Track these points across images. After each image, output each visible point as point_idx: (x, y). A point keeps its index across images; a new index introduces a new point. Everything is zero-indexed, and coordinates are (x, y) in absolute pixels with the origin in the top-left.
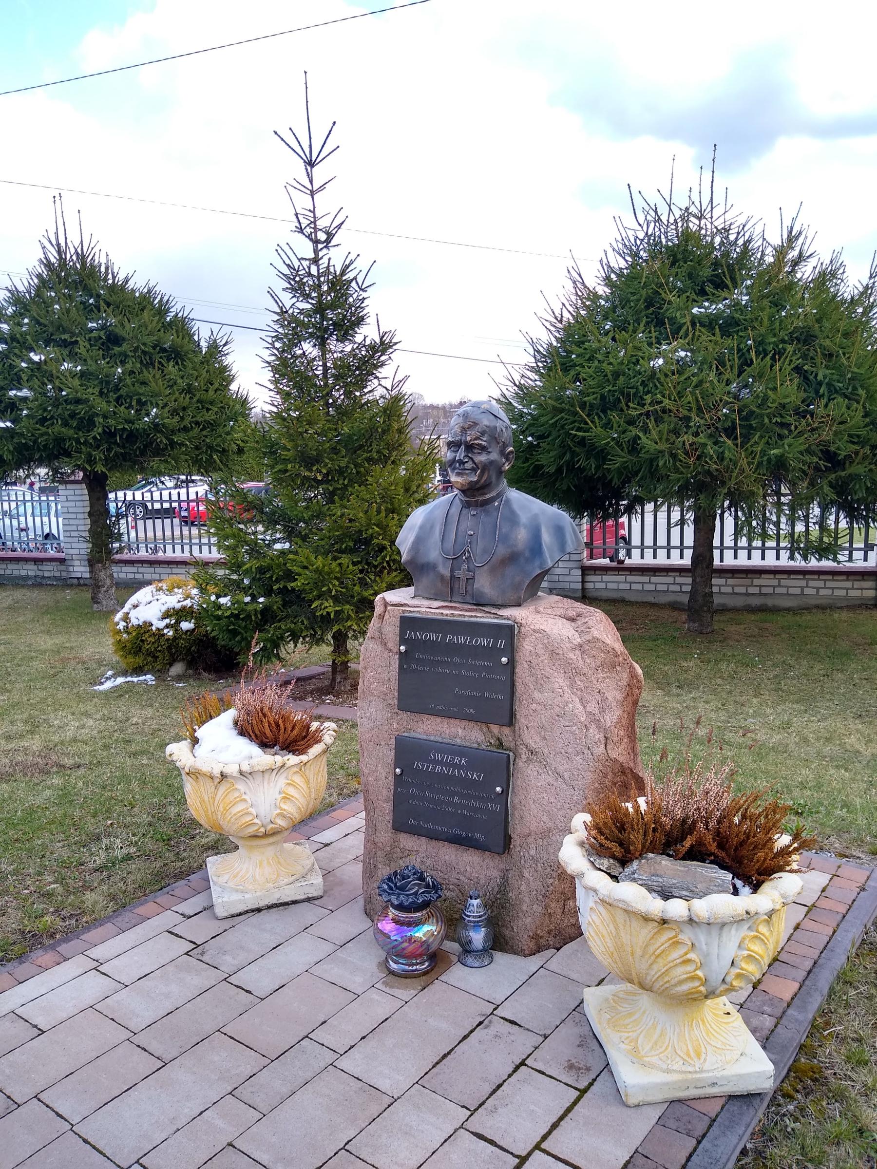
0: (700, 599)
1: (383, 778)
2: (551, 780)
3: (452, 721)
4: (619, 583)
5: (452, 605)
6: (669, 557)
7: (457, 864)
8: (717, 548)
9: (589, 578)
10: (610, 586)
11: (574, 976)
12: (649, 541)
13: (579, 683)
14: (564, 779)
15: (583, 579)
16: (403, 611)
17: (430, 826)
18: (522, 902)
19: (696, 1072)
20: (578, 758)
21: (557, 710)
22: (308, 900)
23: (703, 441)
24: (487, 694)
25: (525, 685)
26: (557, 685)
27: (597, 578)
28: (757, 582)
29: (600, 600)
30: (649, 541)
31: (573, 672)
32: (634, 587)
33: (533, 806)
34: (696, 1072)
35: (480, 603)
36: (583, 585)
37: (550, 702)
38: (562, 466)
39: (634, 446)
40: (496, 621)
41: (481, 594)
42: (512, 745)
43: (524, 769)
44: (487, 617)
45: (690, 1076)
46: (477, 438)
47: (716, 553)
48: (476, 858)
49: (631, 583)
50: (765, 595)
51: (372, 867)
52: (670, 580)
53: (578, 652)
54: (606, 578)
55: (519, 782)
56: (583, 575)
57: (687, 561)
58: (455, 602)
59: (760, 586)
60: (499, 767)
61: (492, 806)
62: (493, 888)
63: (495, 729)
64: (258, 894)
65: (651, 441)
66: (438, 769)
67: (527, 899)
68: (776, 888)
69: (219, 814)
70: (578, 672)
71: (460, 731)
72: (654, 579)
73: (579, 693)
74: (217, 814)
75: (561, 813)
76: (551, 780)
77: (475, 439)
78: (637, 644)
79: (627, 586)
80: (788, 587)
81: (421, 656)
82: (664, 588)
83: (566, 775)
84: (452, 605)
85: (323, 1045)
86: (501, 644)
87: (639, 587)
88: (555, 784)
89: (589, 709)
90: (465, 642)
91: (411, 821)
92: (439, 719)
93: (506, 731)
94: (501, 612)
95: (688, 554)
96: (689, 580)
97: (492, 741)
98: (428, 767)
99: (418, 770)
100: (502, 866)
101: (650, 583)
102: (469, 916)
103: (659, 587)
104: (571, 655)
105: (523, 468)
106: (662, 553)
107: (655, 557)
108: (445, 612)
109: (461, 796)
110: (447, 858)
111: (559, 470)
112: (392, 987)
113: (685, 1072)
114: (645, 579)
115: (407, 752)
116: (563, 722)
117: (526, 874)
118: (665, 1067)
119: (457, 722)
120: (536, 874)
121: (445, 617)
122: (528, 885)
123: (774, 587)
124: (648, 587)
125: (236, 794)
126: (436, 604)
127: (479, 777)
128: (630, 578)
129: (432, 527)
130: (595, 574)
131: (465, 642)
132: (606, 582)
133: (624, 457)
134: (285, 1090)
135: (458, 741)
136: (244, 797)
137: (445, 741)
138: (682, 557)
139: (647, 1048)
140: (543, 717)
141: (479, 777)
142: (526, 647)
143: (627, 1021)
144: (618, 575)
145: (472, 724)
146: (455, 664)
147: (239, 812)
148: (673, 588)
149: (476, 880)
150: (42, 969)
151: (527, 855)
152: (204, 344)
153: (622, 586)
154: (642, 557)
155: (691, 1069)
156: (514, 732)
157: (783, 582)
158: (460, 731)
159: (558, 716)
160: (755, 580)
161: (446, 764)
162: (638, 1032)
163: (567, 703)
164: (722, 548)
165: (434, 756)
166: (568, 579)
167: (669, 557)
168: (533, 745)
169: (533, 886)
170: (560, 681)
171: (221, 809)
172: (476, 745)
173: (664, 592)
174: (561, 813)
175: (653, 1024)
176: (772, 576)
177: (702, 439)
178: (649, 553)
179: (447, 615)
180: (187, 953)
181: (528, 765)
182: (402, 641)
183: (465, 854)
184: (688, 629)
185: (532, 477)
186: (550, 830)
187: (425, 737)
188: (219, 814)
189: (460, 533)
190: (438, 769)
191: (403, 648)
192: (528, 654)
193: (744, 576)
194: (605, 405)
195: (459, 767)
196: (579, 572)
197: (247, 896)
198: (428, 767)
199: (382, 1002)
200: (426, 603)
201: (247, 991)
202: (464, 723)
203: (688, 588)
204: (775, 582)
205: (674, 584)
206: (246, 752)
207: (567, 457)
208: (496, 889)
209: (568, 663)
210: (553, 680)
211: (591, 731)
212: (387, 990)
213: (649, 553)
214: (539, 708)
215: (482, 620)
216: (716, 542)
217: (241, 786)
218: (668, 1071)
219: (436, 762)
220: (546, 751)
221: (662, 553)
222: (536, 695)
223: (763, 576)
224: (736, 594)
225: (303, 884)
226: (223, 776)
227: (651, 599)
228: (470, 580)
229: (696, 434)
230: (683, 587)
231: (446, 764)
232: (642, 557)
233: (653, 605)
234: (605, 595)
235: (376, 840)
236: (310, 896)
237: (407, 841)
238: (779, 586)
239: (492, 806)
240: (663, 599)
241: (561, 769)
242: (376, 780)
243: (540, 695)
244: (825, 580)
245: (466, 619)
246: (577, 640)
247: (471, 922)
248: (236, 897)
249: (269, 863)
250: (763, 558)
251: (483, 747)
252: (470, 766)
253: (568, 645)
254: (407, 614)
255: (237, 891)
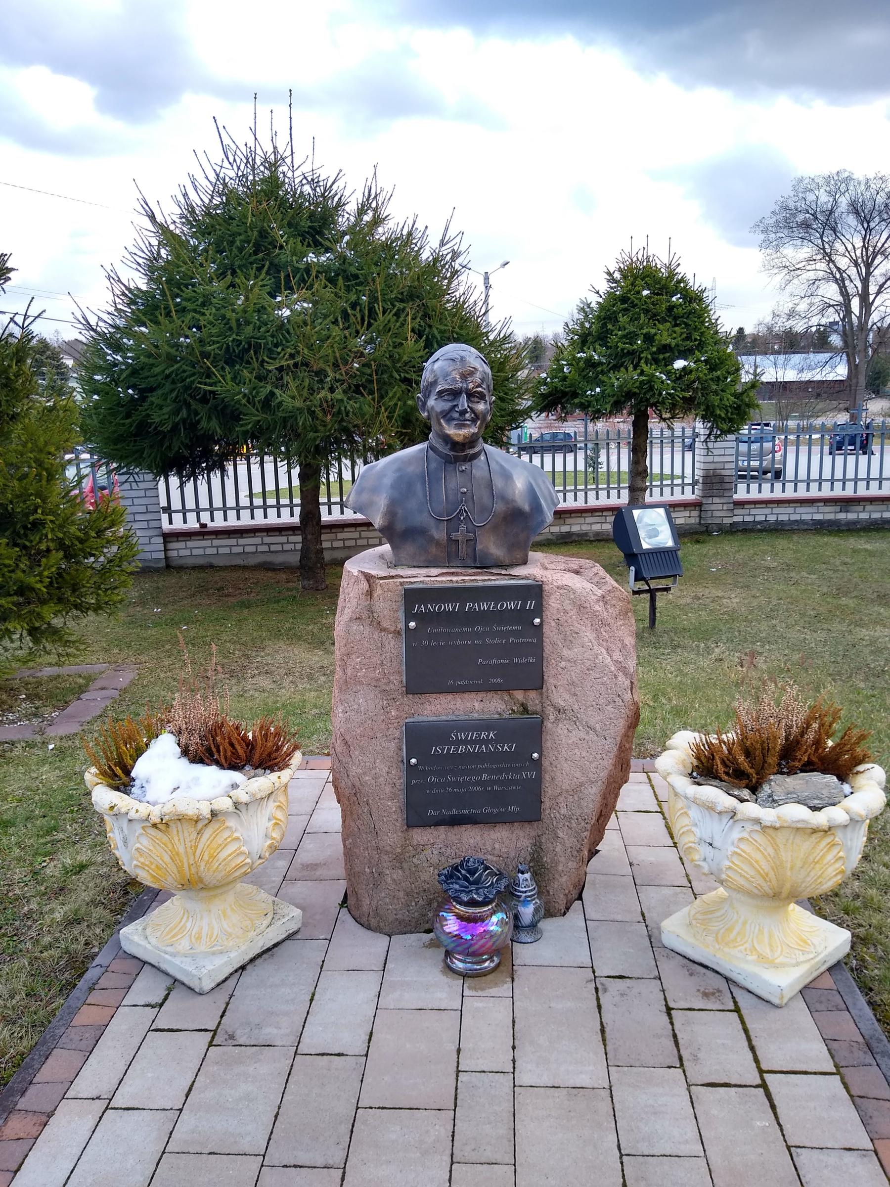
0: (313, 556)
1: (385, 774)
2: (582, 734)
3: (466, 695)
4: (204, 548)
5: (453, 570)
6: (253, 517)
7: (484, 845)
8: (297, 505)
9: (172, 545)
10: (195, 552)
11: (619, 917)
12: (231, 502)
13: (604, 633)
14: (595, 731)
15: (165, 547)
16: (401, 584)
17: (454, 811)
18: (557, 863)
19: (815, 957)
20: (609, 708)
21: (588, 664)
22: (290, 937)
23: (339, 397)
24: (516, 660)
25: (554, 644)
26: (586, 639)
27: (181, 545)
28: (340, 536)
29: (187, 568)
30: (231, 502)
31: (598, 624)
32: (221, 551)
33: (566, 765)
34: (815, 957)
35: (484, 565)
36: (165, 554)
37: (580, 657)
38: (178, 424)
39: (267, 403)
40: (512, 582)
41: (486, 554)
42: (539, 708)
43: (554, 730)
44: (502, 579)
45: (813, 962)
46: (479, 386)
47: (324, 510)
48: (504, 832)
49: (217, 547)
50: (349, 547)
51: (376, 875)
52: (257, 540)
53: (601, 604)
54: (190, 544)
55: (549, 744)
56: (165, 543)
57: (296, 519)
58: (453, 567)
59: (344, 540)
60: (528, 732)
61: (527, 775)
62: (525, 858)
63: (519, 695)
64: (243, 948)
65: (289, 398)
66: (462, 749)
67: (562, 859)
68: (871, 778)
69: (203, 864)
70: (604, 623)
71: (476, 704)
72: (242, 541)
73: (604, 643)
74: (198, 866)
75: (593, 765)
76: (582, 734)
77: (477, 387)
78: (264, 608)
79: (214, 551)
80: (368, 538)
81: (499, 629)
82: (279, 548)
83: (598, 727)
84: (453, 570)
85: (484, 1072)
86: (531, 605)
87: (226, 550)
88: (587, 738)
89: (615, 658)
90: (489, 608)
91: (431, 812)
92: (450, 697)
93: (533, 694)
94: (515, 571)
95: (297, 511)
96: (299, 538)
97: (515, 708)
98: (449, 750)
99: (437, 756)
100: (533, 833)
101: (237, 545)
102: (523, 892)
103: (248, 549)
104: (597, 608)
105: (123, 424)
106: (245, 514)
107: (238, 518)
108: (455, 579)
109: (491, 772)
110: (472, 841)
111: (175, 429)
112: (483, 989)
113: (809, 960)
114: (233, 542)
115: (419, 738)
116: (594, 674)
117: (561, 835)
118: (794, 961)
119: (473, 695)
120: (570, 831)
121: (456, 585)
122: (563, 844)
123: (356, 539)
124: (236, 550)
125: (226, 834)
126: (434, 571)
127: (510, 748)
128: (216, 542)
129: (531, 485)
130: (178, 541)
131: (489, 608)
132: (191, 549)
133: (258, 416)
134: (504, 1130)
135: (475, 715)
136: (236, 835)
137: (461, 718)
138: (292, 515)
139: (768, 951)
140: (572, 673)
141: (510, 748)
142: (553, 604)
143: (732, 936)
144: (204, 539)
145: (490, 694)
146: (477, 633)
147: (230, 855)
148: (262, 548)
149: (505, 855)
150: (26, 1145)
151: (558, 815)
152: (425, 255)
153: (209, 551)
154: (225, 519)
155: (811, 956)
156: (541, 694)
157: (364, 534)
158: (476, 704)
159: (588, 669)
160: (339, 534)
161: (472, 742)
162: (750, 940)
163: (597, 655)
164: (329, 504)
165: (457, 736)
166: (147, 548)
167: (253, 517)
168: (562, 703)
169: (568, 844)
170: (588, 635)
171: (206, 857)
172: (497, 716)
173: (252, 553)
174: (593, 765)
175: (759, 930)
176: (353, 529)
177: (338, 395)
178: (232, 514)
179: (457, 582)
180: (211, 1044)
181: (558, 725)
182: (409, 617)
183: (492, 832)
184: (303, 587)
185: (136, 435)
186: (582, 784)
187: (435, 719)
188: (203, 864)
189: (450, 492)
190: (462, 749)
191: (412, 624)
192: (555, 612)
193: (278, 533)
194: (234, 357)
195: (487, 742)
196: (161, 540)
197: (232, 955)
198: (449, 750)
199: (489, 1008)
200: (424, 571)
201: (339, 1055)
202: (481, 695)
203: (299, 547)
204: (356, 535)
205: (262, 544)
206: (212, 784)
207: (184, 413)
208: (529, 858)
209: (595, 615)
210: (582, 634)
211: (620, 679)
212: (480, 993)
213: (232, 514)
214: (568, 665)
215: (497, 583)
216: (323, 499)
217: (231, 823)
218: (797, 964)
219: (459, 742)
220: (576, 707)
221: (245, 514)
222: (566, 652)
223: (346, 530)
224: (273, 552)
225: (284, 920)
226: (214, 814)
227: (241, 562)
228: (472, 542)
229: (332, 390)
230: (271, 546)
231: (472, 742)
232: (225, 519)
233: (245, 568)
234: (191, 562)
235: (381, 844)
236: (291, 932)
237: (420, 836)
238: (360, 538)
239: (527, 775)
240: (252, 561)
241: (592, 722)
242: (375, 778)
243: (569, 652)
244: (772, 508)
245: (480, 584)
246: (599, 593)
247: (529, 896)
248: (219, 961)
249: (232, 909)
250: (238, 518)
251: (506, 716)
252: (499, 740)
253: (593, 597)
254: (407, 586)
255: (214, 954)
